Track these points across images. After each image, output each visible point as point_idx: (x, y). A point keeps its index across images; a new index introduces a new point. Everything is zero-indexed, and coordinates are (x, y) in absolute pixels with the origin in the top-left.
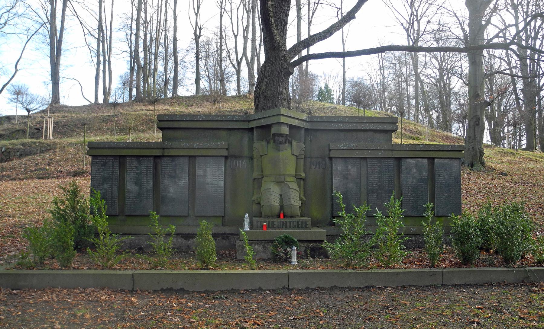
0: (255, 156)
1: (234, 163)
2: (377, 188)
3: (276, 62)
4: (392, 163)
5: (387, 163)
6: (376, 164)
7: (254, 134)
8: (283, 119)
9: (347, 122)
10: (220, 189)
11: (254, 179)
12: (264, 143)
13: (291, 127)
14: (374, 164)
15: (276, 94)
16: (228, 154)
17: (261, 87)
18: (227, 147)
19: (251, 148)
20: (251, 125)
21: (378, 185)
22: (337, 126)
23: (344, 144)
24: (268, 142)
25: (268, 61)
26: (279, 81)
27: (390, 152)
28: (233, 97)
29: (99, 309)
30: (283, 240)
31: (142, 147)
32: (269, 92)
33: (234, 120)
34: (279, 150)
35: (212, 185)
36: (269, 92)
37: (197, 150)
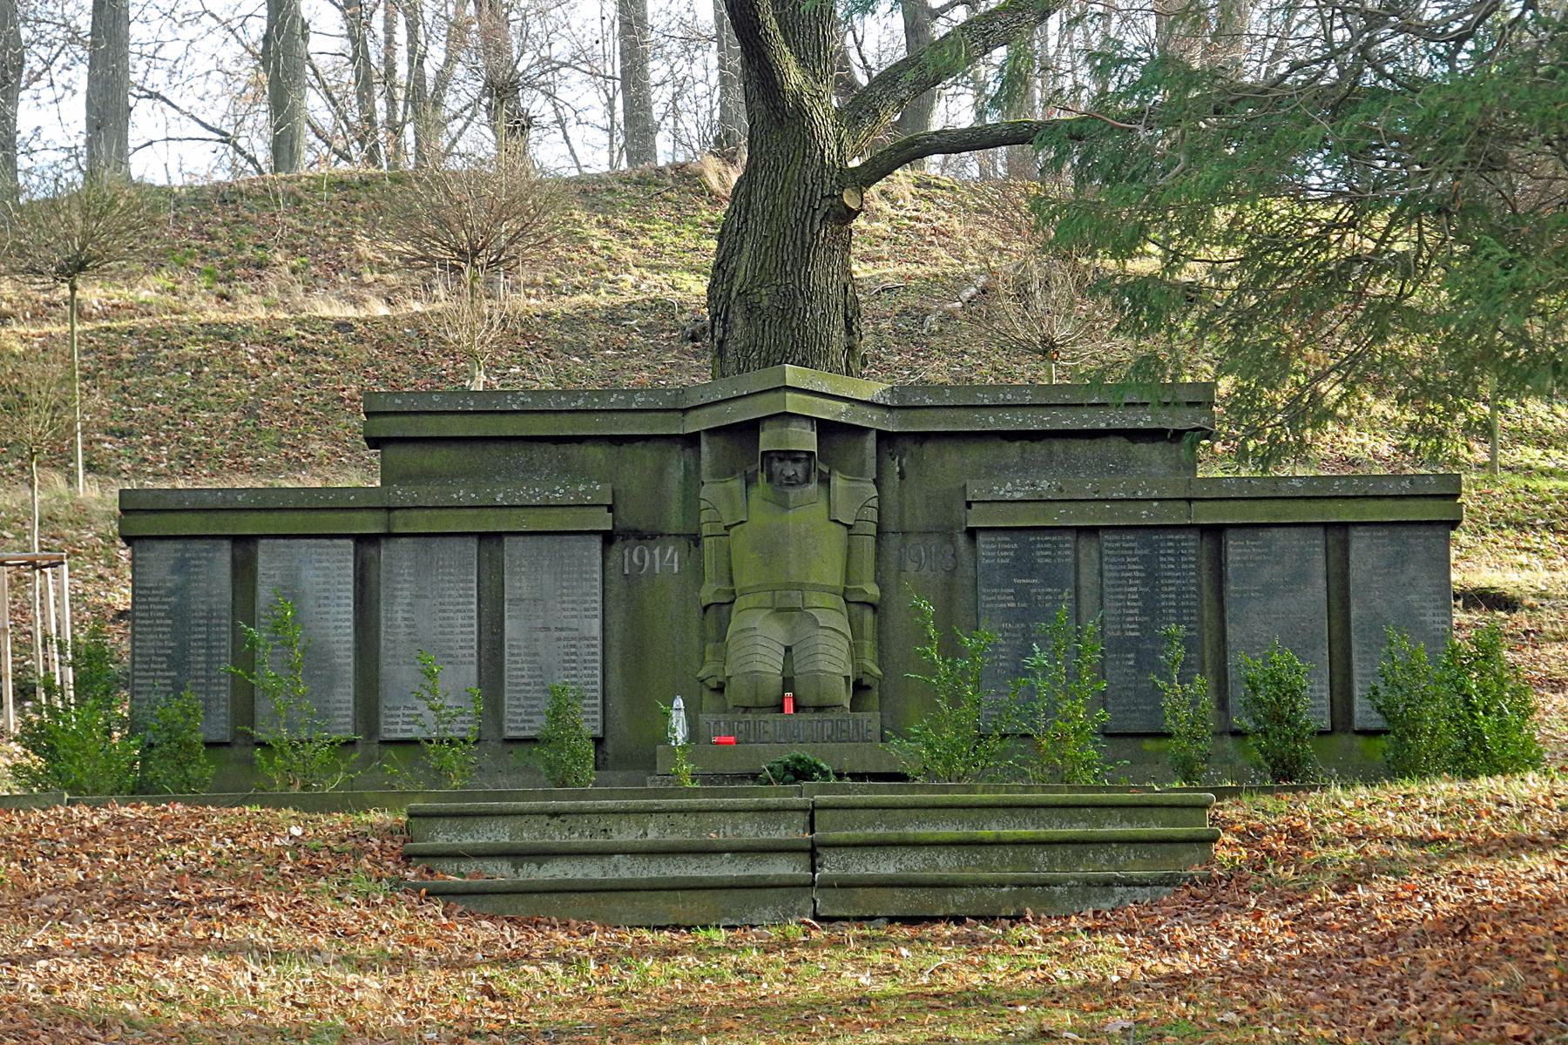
0: (706, 529)
1: (635, 560)
2: (1137, 634)
3: (789, 174)
4: (1192, 544)
5: (1171, 544)
6: (1133, 549)
7: (703, 456)
8: (792, 403)
9: (1030, 405)
10: (588, 646)
11: (706, 609)
12: (737, 484)
13: (826, 429)
14: (1128, 549)
15: (795, 296)
16: (614, 525)
17: (735, 269)
18: (610, 503)
19: (691, 503)
20: (691, 425)
21: (1139, 623)
22: (991, 419)
23: (1014, 484)
24: (750, 482)
25: (760, 165)
26: (803, 247)
27: (1184, 505)
28: (589, 191)
29: (598, 487)
30: (786, 767)
31: (313, 506)
32: (764, 292)
33: (634, 406)
34: (785, 506)
35: (557, 634)
36: (764, 292)
37: (507, 511)
